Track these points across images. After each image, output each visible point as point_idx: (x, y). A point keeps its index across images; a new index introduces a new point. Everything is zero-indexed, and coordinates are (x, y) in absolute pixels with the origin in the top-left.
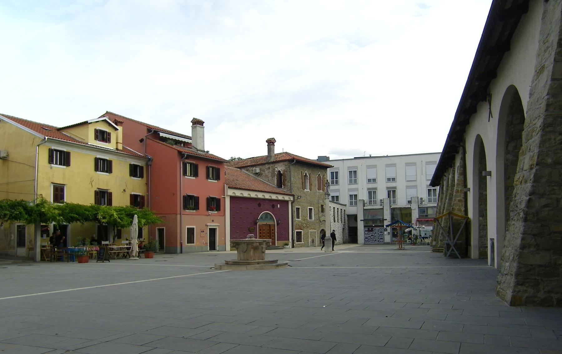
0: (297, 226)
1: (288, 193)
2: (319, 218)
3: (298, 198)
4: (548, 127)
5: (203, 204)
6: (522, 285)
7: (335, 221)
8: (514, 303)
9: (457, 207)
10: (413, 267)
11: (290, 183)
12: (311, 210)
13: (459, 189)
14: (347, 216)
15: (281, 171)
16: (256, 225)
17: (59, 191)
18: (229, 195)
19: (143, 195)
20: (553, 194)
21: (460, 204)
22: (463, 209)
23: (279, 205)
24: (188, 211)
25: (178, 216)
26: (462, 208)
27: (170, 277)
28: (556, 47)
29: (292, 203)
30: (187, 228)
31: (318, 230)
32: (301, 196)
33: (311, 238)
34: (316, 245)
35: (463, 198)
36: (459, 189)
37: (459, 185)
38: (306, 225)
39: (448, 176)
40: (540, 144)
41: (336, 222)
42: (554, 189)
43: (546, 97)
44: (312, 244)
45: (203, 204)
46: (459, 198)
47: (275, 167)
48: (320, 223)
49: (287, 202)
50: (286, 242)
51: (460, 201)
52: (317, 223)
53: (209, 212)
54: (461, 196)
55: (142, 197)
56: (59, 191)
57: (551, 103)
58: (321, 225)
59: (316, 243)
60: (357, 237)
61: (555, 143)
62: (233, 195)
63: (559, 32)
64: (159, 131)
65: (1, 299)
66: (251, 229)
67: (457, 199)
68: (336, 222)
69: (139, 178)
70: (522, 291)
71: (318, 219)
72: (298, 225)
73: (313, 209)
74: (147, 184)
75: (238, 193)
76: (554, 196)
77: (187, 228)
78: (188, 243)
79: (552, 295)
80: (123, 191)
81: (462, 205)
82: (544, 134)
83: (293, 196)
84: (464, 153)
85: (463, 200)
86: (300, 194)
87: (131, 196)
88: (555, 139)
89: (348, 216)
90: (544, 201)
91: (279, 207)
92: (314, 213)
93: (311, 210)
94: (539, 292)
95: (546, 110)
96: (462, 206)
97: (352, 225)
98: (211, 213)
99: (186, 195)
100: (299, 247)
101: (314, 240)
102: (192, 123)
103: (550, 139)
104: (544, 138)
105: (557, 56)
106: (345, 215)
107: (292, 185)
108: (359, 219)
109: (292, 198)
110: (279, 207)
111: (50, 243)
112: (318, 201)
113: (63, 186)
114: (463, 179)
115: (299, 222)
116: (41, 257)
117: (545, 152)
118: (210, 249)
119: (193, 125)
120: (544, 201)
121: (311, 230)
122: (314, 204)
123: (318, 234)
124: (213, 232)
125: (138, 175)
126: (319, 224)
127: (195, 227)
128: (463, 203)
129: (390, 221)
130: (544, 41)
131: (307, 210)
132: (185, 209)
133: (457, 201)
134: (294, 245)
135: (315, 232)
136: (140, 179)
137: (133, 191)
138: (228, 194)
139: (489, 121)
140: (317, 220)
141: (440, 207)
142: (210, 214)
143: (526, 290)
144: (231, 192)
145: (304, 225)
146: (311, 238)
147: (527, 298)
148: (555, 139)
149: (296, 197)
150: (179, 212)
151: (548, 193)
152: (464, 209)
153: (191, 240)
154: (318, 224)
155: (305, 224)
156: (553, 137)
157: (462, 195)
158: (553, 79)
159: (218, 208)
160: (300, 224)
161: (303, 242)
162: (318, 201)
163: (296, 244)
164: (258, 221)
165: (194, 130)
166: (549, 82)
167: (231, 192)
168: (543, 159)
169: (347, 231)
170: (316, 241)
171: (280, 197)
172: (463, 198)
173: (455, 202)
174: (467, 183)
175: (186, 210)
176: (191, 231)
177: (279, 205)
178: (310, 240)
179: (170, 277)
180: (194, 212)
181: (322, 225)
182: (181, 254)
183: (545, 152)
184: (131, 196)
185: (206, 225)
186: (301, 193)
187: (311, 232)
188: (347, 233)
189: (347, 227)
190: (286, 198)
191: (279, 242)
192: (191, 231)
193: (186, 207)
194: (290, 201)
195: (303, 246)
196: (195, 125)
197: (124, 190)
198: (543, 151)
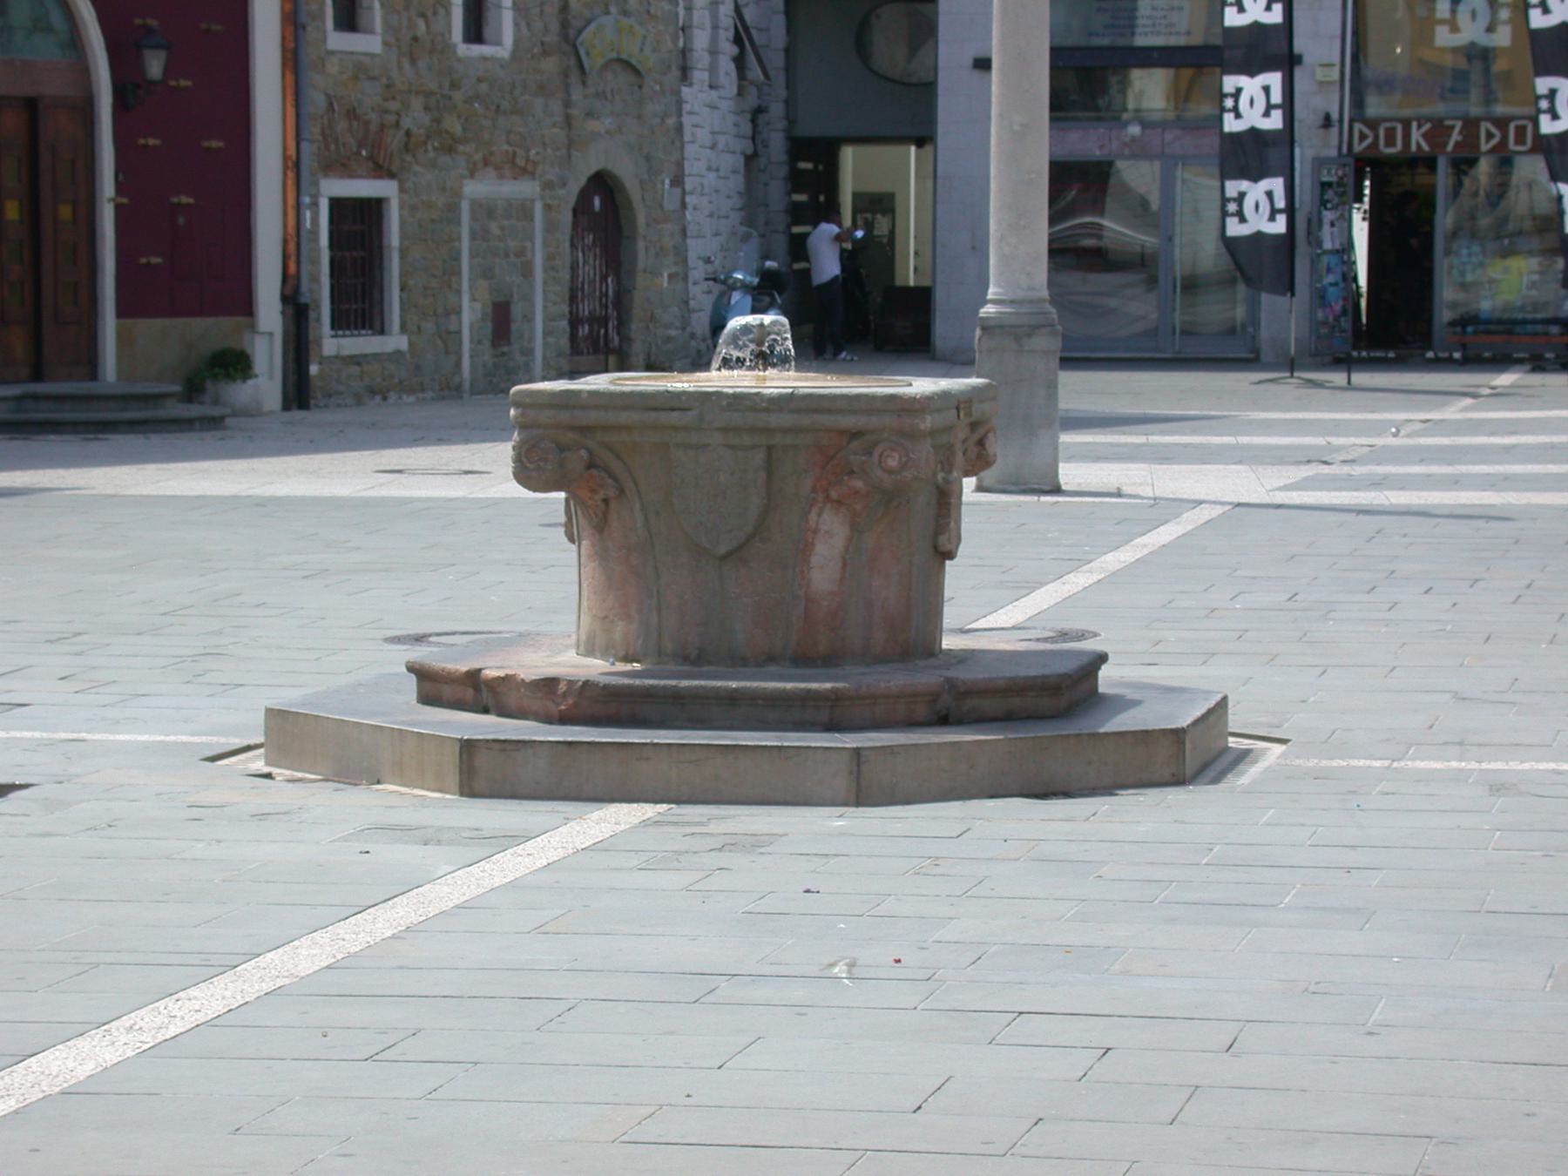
0: (342, 125)
2: (565, 37)
23: (221, 144)
27: (1445, 441)
38: (426, 119)
50: (209, 331)
52: (542, 89)
58: (590, 115)
65: (2, 734)
71: (552, 38)
91: (809, 166)
100: (359, 401)
101: (517, 310)
110: (809, 166)
111: (828, 221)
115: (360, 69)
116: (572, 347)
121: (478, 188)
123: (550, 227)
126: (567, 104)
134: (314, 369)
135: (525, 212)
140: (545, 53)
145: (416, 118)
154: (556, 106)
155: (417, 103)
160: (369, 96)
161: (396, 341)
163: (322, 361)
170: (529, 318)
178: (470, 314)
179: (1445, 441)
181: (593, 125)
182: (298, 415)
187: (485, 210)
191: (149, 328)
195: (404, 388)
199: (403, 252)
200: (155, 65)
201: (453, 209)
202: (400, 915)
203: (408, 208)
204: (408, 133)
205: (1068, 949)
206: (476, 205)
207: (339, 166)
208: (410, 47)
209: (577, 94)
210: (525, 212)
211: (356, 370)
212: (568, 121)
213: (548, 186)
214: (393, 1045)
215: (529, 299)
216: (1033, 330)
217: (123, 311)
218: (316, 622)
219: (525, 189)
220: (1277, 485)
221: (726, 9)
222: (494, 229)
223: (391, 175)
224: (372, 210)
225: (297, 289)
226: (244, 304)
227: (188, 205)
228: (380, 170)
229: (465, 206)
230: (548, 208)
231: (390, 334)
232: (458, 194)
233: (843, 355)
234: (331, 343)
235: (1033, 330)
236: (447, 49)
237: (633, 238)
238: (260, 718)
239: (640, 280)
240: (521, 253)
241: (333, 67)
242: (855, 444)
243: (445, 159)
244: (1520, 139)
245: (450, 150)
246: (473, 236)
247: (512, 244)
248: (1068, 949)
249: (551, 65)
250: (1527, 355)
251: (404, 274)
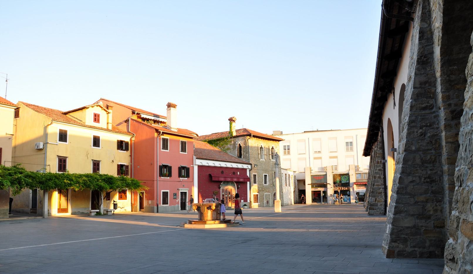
1: (247, 162)
3: (255, 166)
4: (412, 123)
5: (175, 172)
6: (395, 242)
7: (286, 186)
8: (390, 254)
9: (378, 175)
11: (248, 154)
12: (266, 176)
13: (379, 161)
14: (297, 181)
15: (240, 144)
16: (219, 189)
17: (62, 162)
18: (197, 165)
19: (128, 164)
20: (417, 173)
21: (380, 172)
22: (382, 177)
23: (238, 172)
24: (163, 178)
25: (155, 182)
26: (381, 176)
28: (416, 64)
29: (250, 171)
30: (163, 192)
31: (272, 192)
32: (257, 165)
33: (266, 200)
34: (270, 205)
35: (382, 168)
36: (379, 161)
37: (379, 157)
39: (375, 149)
40: (406, 136)
41: (288, 186)
42: (417, 170)
43: (410, 101)
44: (267, 204)
45: (175, 172)
46: (379, 168)
47: (236, 141)
48: (274, 187)
49: (246, 169)
51: (379, 170)
53: (181, 178)
54: (380, 166)
55: (127, 167)
56: (62, 162)
57: (414, 105)
59: (270, 204)
61: (417, 135)
62: (200, 164)
63: (418, 53)
64: (140, 113)
66: (215, 192)
67: (378, 168)
68: (288, 186)
69: (125, 151)
70: (395, 246)
71: (272, 184)
72: (255, 189)
73: (268, 176)
74: (131, 156)
75: (205, 163)
76: (417, 174)
77: (163, 192)
78: (163, 204)
79: (416, 249)
80: (111, 161)
81: (382, 173)
82: (409, 128)
83: (251, 164)
84: (383, 132)
85: (382, 169)
86: (256, 163)
87: (118, 165)
88: (417, 132)
89: (298, 180)
90: (410, 178)
91: (239, 174)
92: (269, 179)
93: (266, 176)
94: (407, 247)
95: (410, 110)
96: (382, 174)
97: (301, 189)
98: (182, 179)
99: (161, 165)
101: (269, 201)
102: (167, 106)
103: (414, 132)
104: (409, 131)
105: (416, 70)
106: (296, 180)
107: (250, 156)
108: (307, 183)
109: (249, 166)
110: (239, 174)
112: (272, 169)
113: (66, 158)
114: (382, 152)
117: (410, 141)
118: (182, 209)
119: (168, 108)
120: (410, 178)
122: (268, 171)
124: (184, 194)
125: (124, 149)
126: (273, 188)
127: (168, 191)
128: (382, 172)
130: (412, 59)
131: (263, 176)
132: (161, 177)
133: (378, 170)
135: (270, 195)
136: (125, 152)
137: (120, 161)
138: (197, 164)
139: (394, 109)
140: (271, 184)
141: (370, 173)
142: (181, 180)
143: (398, 246)
144: (199, 162)
146: (266, 200)
147: (398, 252)
148: (417, 132)
149: (253, 165)
150: (155, 179)
151: (413, 173)
152: (383, 177)
153: (165, 202)
154: (272, 188)
155: (260, 188)
156: (416, 130)
157: (382, 165)
158: (414, 88)
159: (188, 176)
162: (272, 169)
164: (221, 186)
165: (168, 111)
166: (412, 90)
167: (199, 162)
168: (409, 147)
169: (297, 193)
170: (270, 202)
171: (240, 166)
172: (382, 168)
173: (376, 171)
174: (385, 156)
175: (162, 177)
176: (165, 194)
177: (238, 172)
178: (265, 202)
180: (168, 179)
183: (410, 141)
184: (118, 165)
185: (178, 189)
186: (257, 162)
188: (298, 195)
189: (297, 190)
190: (245, 166)
192: (165, 194)
193: (161, 175)
194: (248, 169)
196: (170, 108)
197: (113, 161)
198: (409, 141)
201: (263, 195)
202: (448, 228)
203: (260, 195)
206: (265, 195)
209: (274, 187)
210: (270, 195)
212: (273, 189)
215: (270, 201)
217: (57, 133)
219: (270, 193)
220: (81, 211)
221: (1, 216)
230: (271, 195)
232: (264, 194)
233: (217, 147)
238: (235, 215)
249: (272, 185)
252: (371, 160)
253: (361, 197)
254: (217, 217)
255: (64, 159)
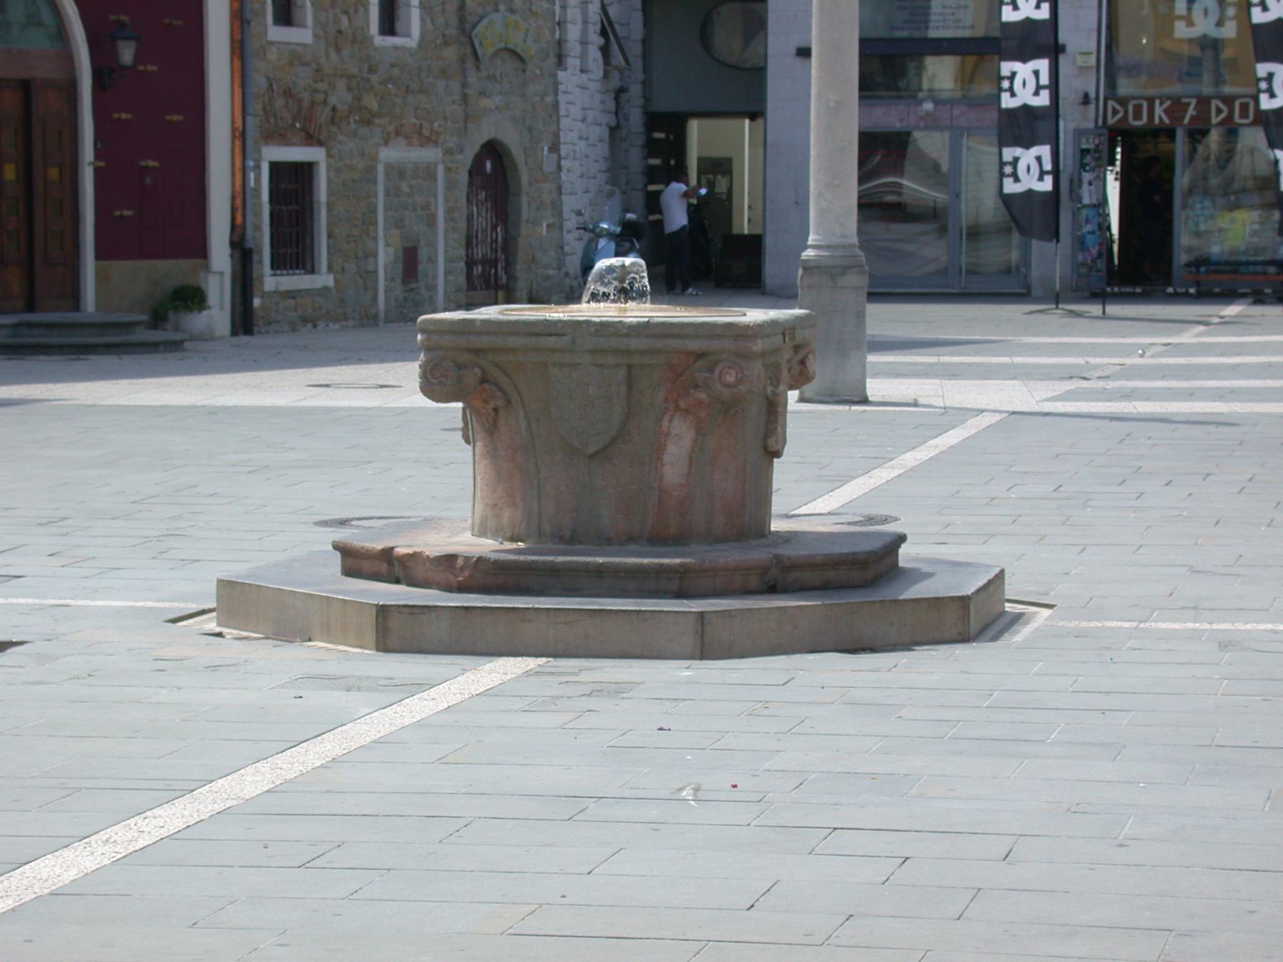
0: (279, 102)
2: (462, 30)
10: (1206, 626)
23: (181, 118)
27: (1183, 361)
38: (349, 98)
50: (171, 271)
52: (444, 73)
58: (483, 94)
60: (355, 363)
71: (452, 31)
91: (662, 135)
100: (294, 328)
101: (423, 254)
110: (662, 135)
115: (295, 57)
121: (391, 154)
123: (450, 186)
126: (464, 85)
129: (1092, 61)
134: (257, 302)
135: (430, 173)
140: (446, 43)
145: (340, 97)
154: (455, 87)
155: (341, 84)
160: (302, 79)
161: (324, 279)
163: (264, 295)
170: (432, 260)
178: (385, 257)
179: (1183, 361)
181: (485, 102)
187: (397, 172)
191: (122, 268)
195: (331, 317)
199: (330, 206)
200: (127, 53)
201: (370, 171)
203: (334, 170)
204: (334, 109)
205: (874, 776)
206: (390, 168)
207: (277, 136)
208: (336, 39)
209: (472, 77)
210: (430, 173)
211: (291, 303)
212: (465, 99)
213: (448, 152)
214: (322, 855)
215: (432, 245)
216: (845, 270)
217: (100, 255)
218: (258, 509)
219: (429, 154)
222: (405, 187)
223: (320, 143)
224: (304, 171)
225: (243, 237)
226: (200, 249)
227: (154, 168)
228: (311, 139)
229: (381, 169)
230: (448, 170)
231: (319, 273)
232: (375, 159)
234: (271, 281)
235: (845, 270)
236: (366, 40)
237: (518, 195)
238: (213, 587)
239: (524, 229)
240: (426, 207)
241: (272, 55)
242: (699, 363)
243: (364, 130)
244: (1244, 114)
245: (368, 123)
246: (387, 193)
247: (419, 200)
248: (874, 776)
249: (450, 53)
250: (1249, 291)
251: (331, 225)
252: (310, 321)
253: (555, 152)
254: (1134, 70)
255: (735, 164)
